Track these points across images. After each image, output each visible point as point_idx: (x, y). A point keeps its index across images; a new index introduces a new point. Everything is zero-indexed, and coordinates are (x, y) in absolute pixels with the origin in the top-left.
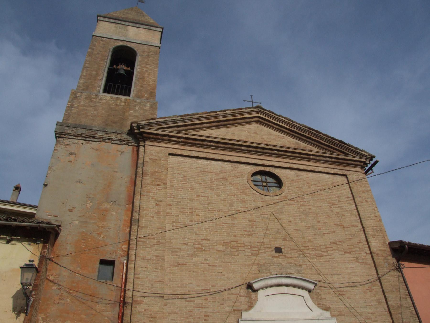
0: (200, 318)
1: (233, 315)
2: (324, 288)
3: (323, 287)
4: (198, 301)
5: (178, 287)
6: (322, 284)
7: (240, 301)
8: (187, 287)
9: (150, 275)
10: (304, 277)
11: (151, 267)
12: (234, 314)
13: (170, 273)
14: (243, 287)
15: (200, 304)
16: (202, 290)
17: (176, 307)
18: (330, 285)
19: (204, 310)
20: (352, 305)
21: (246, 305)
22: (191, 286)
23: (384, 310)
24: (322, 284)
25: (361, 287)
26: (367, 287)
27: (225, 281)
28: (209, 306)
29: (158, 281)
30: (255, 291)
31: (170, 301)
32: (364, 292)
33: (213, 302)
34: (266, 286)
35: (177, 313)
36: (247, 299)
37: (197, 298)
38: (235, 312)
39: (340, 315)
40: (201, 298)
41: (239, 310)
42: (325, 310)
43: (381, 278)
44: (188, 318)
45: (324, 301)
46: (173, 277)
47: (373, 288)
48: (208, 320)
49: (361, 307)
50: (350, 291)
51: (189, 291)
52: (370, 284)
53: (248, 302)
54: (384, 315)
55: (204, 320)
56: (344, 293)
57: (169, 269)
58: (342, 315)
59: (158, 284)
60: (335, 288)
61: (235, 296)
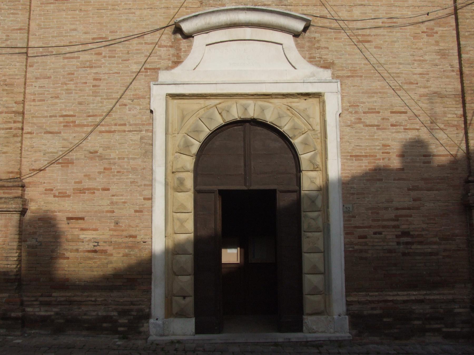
0: (86, 83)
1: (143, 77)
2: (329, 30)
3: (327, 28)
4: (85, 57)
5: (53, 37)
6: (326, 23)
7: (158, 53)
8: (67, 36)
9: (4, 20)
10: (290, 10)
11: (7, 7)
12: (146, 76)
13: (40, 15)
14: (166, 31)
15: (87, 61)
16: (93, 39)
17: (48, 67)
18: (341, 23)
19: (94, 71)
20: (382, 61)
21: (169, 60)
22: (74, 33)
23: (449, 68)
24: (326, 23)
25: (410, 27)
26: (423, 27)
27: (134, 22)
28: (103, 63)
29: (17, 29)
30: (188, 36)
31: (39, 59)
32: (415, 37)
33: (110, 57)
34: (207, 26)
35: (49, 78)
36: (172, 51)
37: (83, 53)
38: (147, 72)
39: (352, 76)
40: (90, 52)
41: (154, 69)
42: (321, 67)
43: (458, 11)
44: (66, 84)
45: (324, 52)
46: (44, 22)
47: (436, 29)
48: (99, 86)
49: (400, 64)
50: (384, 35)
51: (71, 42)
52: (432, 23)
53: (174, 55)
54: (448, 77)
55: (93, 86)
56: (369, 38)
57: (38, 9)
58: (357, 76)
59: (17, 33)
60: (350, 29)
61: (150, 46)
